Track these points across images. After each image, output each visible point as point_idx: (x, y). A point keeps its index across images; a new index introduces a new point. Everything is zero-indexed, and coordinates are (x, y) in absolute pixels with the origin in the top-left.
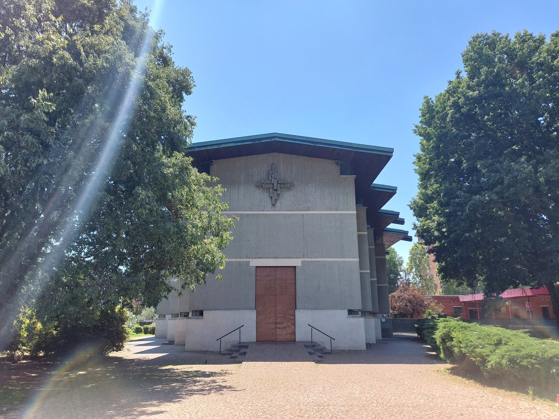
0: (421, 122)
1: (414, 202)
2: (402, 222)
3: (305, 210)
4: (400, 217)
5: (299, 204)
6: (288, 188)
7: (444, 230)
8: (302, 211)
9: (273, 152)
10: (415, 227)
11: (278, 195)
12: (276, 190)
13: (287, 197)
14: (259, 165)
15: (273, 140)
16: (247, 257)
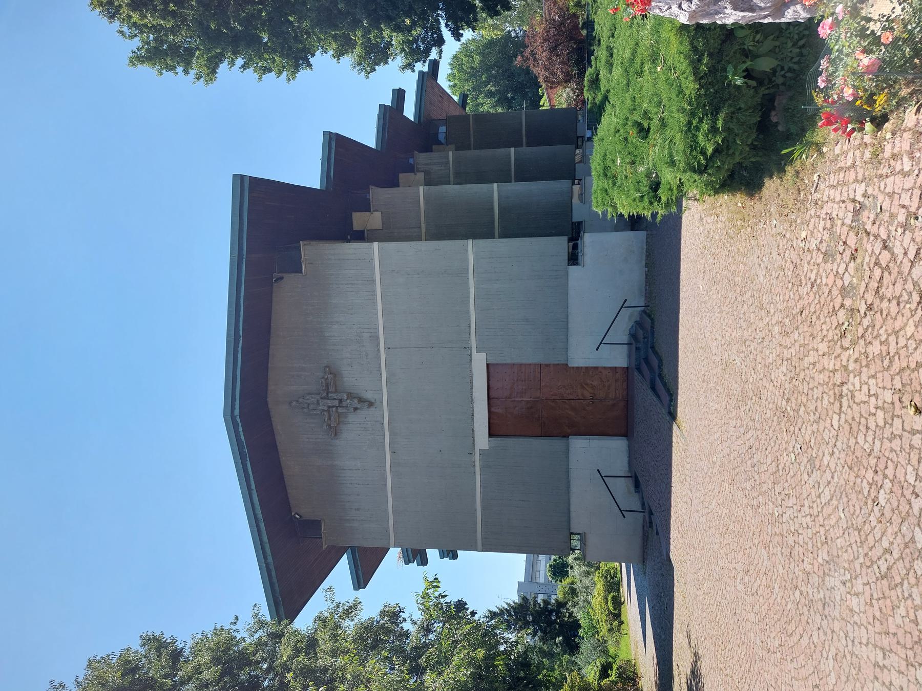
0: (186, 72)
1: (359, 64)
2: (399, 95)
3: (378, 344)
4: (388, 102)
5: (367, 355)
6: (335, 375)
7: (408, 22)
8: (379, 350)
9: (266, 404)
10: (409, 66)
11: (350, 396)
12: (341, 400)
13: (354, 378)
14: (294, 430)
15: (238, 419)
16: (472, 453)
